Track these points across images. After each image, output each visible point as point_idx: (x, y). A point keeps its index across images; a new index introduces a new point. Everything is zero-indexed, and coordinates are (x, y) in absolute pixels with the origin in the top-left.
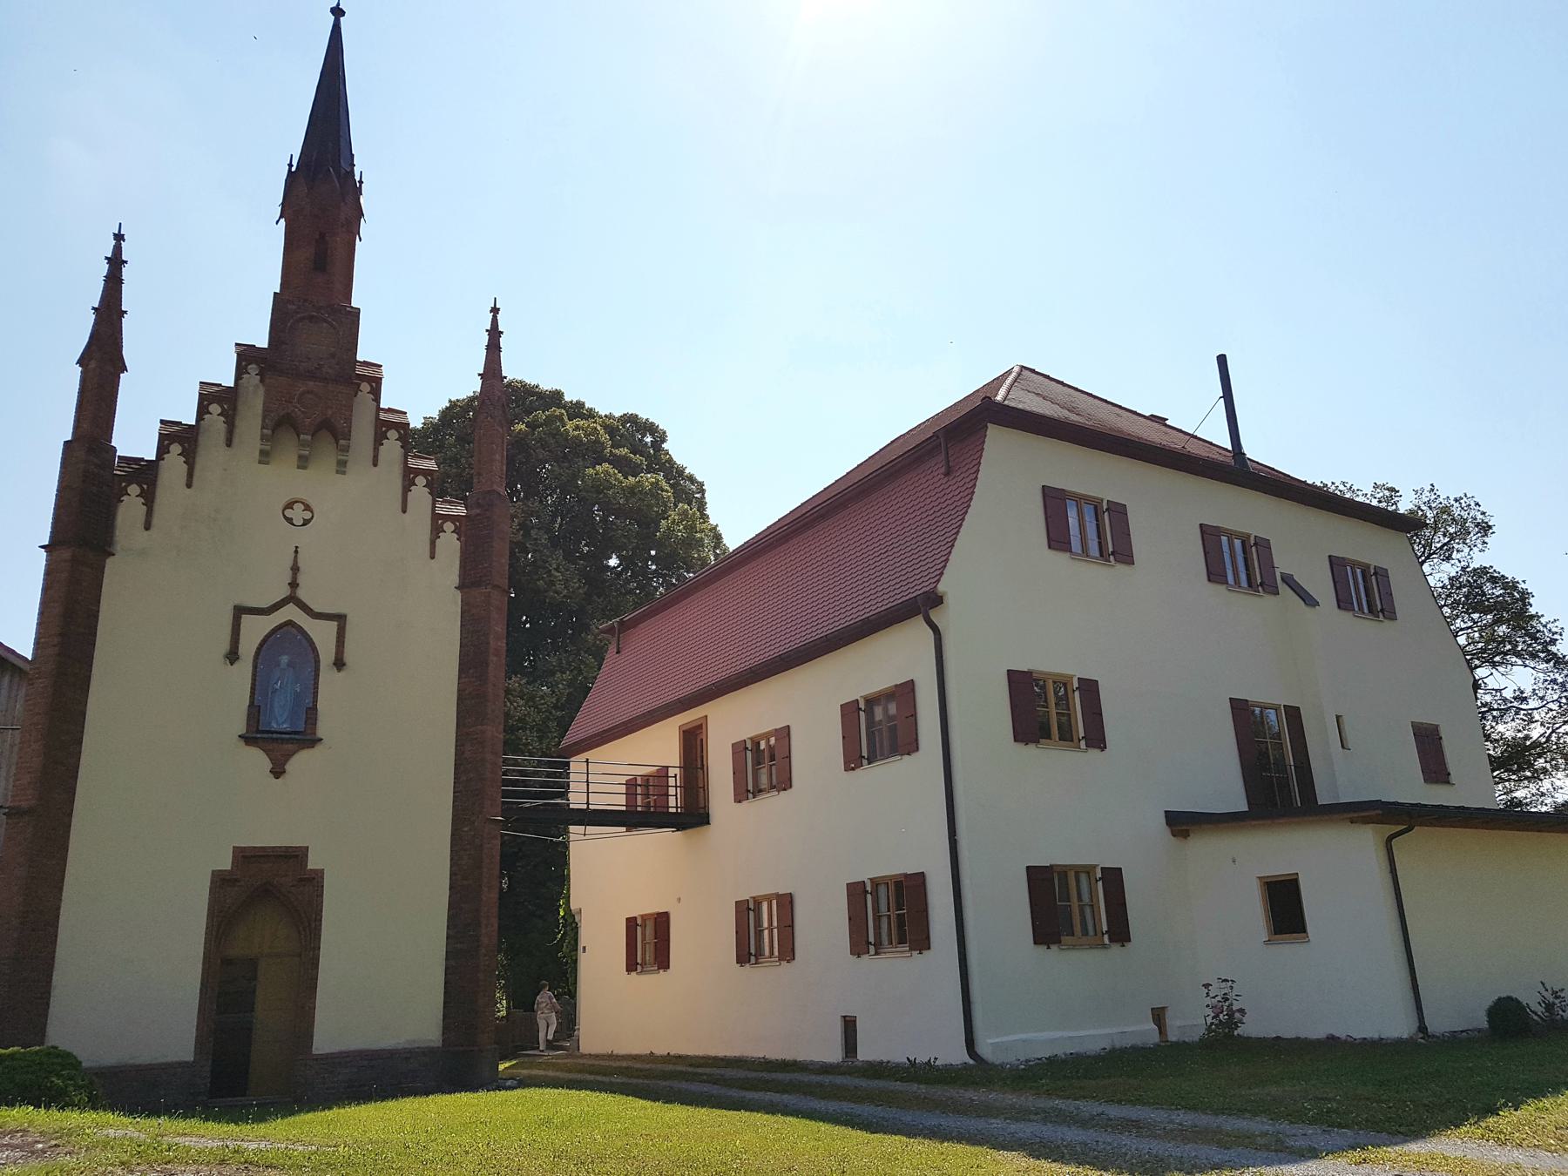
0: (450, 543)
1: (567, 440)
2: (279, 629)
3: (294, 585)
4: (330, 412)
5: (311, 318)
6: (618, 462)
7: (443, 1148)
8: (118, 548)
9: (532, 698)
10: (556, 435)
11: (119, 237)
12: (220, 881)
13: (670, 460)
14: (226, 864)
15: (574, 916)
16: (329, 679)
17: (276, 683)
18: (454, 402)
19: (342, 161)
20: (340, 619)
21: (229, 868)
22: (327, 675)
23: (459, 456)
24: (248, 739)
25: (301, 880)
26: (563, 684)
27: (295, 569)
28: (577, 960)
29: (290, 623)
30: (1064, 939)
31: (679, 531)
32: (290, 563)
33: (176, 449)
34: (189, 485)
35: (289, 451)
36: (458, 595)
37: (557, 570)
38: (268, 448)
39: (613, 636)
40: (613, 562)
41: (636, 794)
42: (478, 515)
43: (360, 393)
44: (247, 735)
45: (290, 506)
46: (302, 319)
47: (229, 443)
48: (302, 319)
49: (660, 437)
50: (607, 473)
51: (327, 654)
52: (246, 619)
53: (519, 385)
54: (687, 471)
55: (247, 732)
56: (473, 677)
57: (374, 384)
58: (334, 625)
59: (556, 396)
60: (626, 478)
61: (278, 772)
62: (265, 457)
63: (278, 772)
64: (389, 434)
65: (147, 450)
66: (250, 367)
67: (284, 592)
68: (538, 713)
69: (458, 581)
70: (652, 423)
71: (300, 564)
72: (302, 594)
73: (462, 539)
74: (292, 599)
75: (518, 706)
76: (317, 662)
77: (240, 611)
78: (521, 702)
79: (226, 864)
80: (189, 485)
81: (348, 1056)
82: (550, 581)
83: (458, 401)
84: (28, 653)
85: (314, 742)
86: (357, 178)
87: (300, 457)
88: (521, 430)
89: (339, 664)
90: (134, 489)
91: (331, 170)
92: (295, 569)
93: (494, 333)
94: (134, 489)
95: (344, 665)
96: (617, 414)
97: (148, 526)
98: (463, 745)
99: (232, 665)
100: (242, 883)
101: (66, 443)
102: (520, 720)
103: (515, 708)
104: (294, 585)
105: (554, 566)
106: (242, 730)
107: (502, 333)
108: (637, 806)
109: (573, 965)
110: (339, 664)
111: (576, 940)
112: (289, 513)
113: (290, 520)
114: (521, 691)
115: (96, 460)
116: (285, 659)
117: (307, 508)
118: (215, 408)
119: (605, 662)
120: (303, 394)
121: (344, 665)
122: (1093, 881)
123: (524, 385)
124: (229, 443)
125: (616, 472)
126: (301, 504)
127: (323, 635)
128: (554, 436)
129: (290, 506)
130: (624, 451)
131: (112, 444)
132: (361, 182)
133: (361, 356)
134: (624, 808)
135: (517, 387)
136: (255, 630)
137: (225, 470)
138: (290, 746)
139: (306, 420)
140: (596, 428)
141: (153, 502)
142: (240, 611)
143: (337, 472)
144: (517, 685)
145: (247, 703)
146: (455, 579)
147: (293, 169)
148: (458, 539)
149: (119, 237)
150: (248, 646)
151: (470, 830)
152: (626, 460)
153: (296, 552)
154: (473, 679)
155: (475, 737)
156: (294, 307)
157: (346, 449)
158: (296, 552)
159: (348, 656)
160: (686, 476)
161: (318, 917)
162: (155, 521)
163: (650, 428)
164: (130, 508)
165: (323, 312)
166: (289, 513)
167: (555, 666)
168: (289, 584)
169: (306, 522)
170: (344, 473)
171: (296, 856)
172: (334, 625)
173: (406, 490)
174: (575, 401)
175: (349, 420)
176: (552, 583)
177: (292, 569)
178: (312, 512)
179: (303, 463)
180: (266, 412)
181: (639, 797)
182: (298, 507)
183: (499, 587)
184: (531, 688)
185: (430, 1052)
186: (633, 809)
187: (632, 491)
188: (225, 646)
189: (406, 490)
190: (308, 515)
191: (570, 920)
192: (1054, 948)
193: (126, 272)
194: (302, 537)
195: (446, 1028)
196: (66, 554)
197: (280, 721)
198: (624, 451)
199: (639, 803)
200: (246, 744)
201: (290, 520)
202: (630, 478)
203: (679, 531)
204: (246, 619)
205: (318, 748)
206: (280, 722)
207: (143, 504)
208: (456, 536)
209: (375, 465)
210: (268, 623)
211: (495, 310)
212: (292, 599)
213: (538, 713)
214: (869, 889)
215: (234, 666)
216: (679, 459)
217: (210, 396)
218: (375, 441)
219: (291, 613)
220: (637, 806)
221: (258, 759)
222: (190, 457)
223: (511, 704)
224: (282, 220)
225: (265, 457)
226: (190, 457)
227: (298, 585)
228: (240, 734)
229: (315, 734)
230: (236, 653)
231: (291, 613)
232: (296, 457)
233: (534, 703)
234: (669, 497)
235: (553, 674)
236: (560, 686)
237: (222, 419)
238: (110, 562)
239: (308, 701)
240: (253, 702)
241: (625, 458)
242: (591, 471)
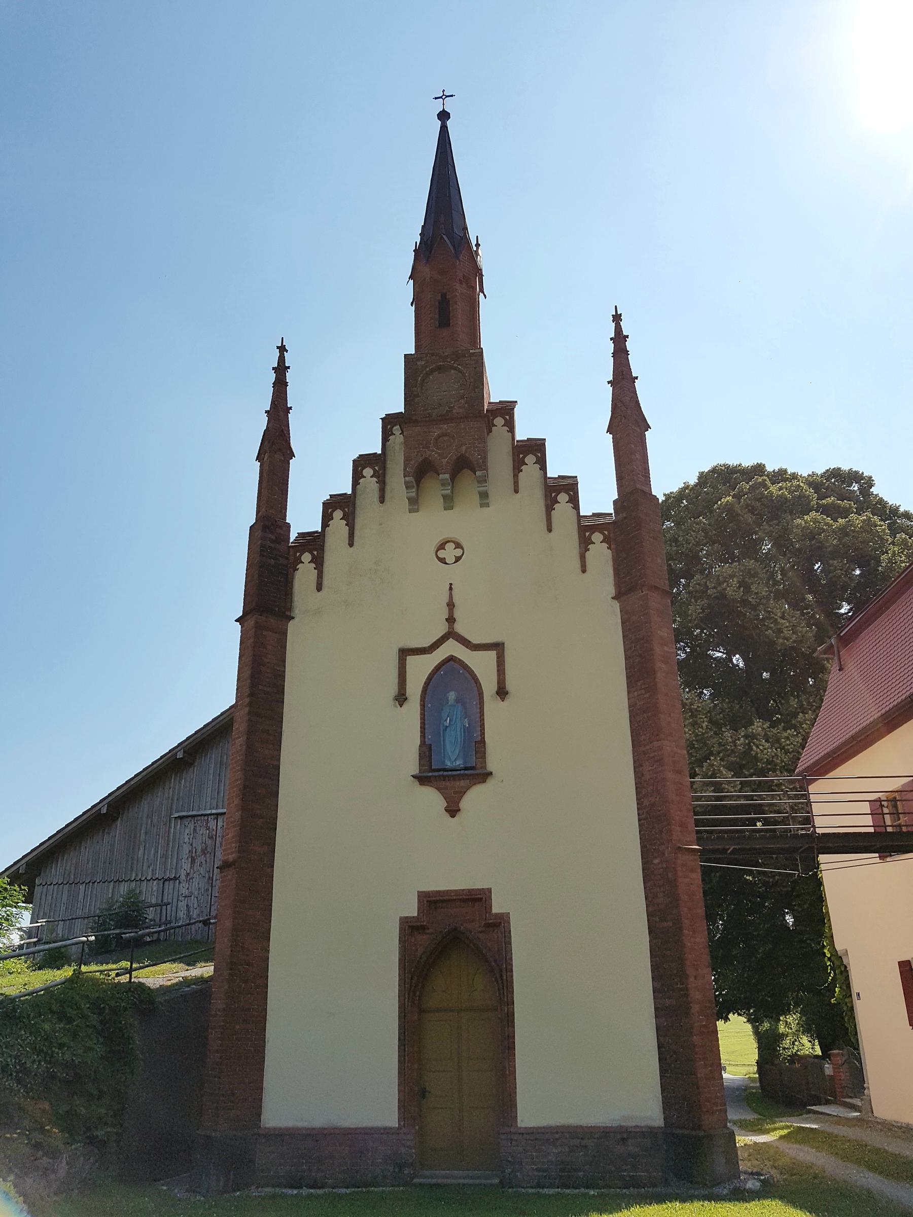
1: (773, 501)
2: (443, 665)
3: (451, 620)
4: (464, 448)
5: (440, 369)
6: (826, 510)
8: (297, 612)
9: (778, 741)
10: (761, 498)
11: (282, 349)
13: (881, 501)
14: (412, 910)
15: (841, 957)
16: (493, 709)
17: (446, 720)
18: (668, 494)
19: (455, 229)
20: (498, 647)
21: (416, 915)
22: (492, 706)
23: (676, 536)
24: (422, 779)
25: (488, 925)
26: (806, 724)
27: (451, 605)
28: (852, 1007)
29: (451, 659)
31: (902, 562)
32: (446, 600)
33: (338, 514)
34: (351, 544)
36: (616, 605)
37: (783, 617)
38: (414, 495)
39: (833, 653)
40: (845, 609)
41: (883, 814)
42: (625, 518)
43: (494, 428)
44: (420, 775)
45: (442, 547)
46: (432, 371)
47: (382, 500)
48: (432, 371)
49: (869, 482)
50: (815, 521)
51: (489, 686)
52: (411, 660)
53: (723, 468)
54: (902, 509)
55: (420, 772)
56: (641, 689)
57: (507, 417)
58: (493, 654)
59: (759, 469)
60: (835, 521)
61: (453, 811)
62: (414, 504)
63: (453, 811)
64: (526, 460)
66: (395, 428)
68: (786, 754)
69: (614, 592)
70: (855, 471)
71: (456, 600)
72: (459, 628)
73: (612, 546)
74: (451, 634)
75: (765, 749)
76: (481, 694)
77: (404, 653)
78: (767, 745)
79: (412, 910)
80: (351, 544)
81: (557, 1133)
82: (777, 628)
83: (671, 493)
85: (484, 776)
86: (474, 243)
87: (445, 497)
88: (728, 501)
89: (502, 692)
90: (306, 557)
91: (446, 239)
92: (451, 605)
93: (620, 339)
95: (507, 693)
96: (820, 471)
97: (319, 588)
98: (641, 765)
99: (401, 707)
100: (431, 931)
102: (769, 762)
103: (762, 751)
104: (451, 620)
105: (779, 614)
106: (416, 771)
107: (627, 337)
108: (886, 826)
109: (849, 1013)
111: (848, 986)
112: (441, 554)
113: (443, 561)
114: (766, 734)
115: (270, 536)
116: (452, 696)
117: (458, 546)
118: (368, 472)
119: (829, 683)
120: (439, 436)
121: (507, 693)
123: (727, 467)
124: (382, 500)
125: (825, 517)
126: (452, 544)
128: (759, 500)
129: (442, 547)
130: (830, 500)
131: (287, 521)
132: (478, 245)
134: (872, 830)
135: (721, 470)
137: (381, 524)
138: (463, 783)
139: (443, 460)
140: (799, 485)
141: (322, 565)
142: (404, 653)
143: (482, 506)
144: (760, 729)
145: (418, 742)
146: (611, 590)
148: (608, 548)
149: (282, 349)
150: (415, 688)
151: (661, 862)
152: (834, 508)
153: (451, 589)
154: (643, 691)
155: (652, 755)
156: (423, 363)
157: (483, 480)
158: (451, 589)
160: (902, 514)
161: (509, 967)
162: (326, 582)
163: (855, 476)
164: (305, 573)
165: (449, 360)
166: (441, 554)
167: (797, 708)
168: (447, 619)
169: (458, 559)
170: (488, 505)
172: (493, 654)
174: (777, 470)
176: (780, 631)
177: (448, 605)
178: (463, 549)
179: (449, 502)
180: (407, 460)
181: (887, 817)
182: (450, 546)
183: (657, 588)
184: (775, 730)
185: (650, 1132)
186: (883, 830)
187: (843, 532)
188: (394, 689)
190: (458, 552)
191: (837, 963)
193: (290, 376)
194: (452, 573)
195: (667, 1104)
196: (251, 622)
197: (453, 758)
198: (830, 500)
199: (888, 822)
200: (420, 784)
201: (443, 561)
202: (840, 520)
203: (902, 562)
204: (411, 660)
205: (490, 784)
206: (453, 760)
207: (315, 569)
208: (606, 545)
209: (516, 491)
210: (430, 662)
211: (617, 318)
212: (451, 634)
213: (786, 754)
215: (404, 706)
216: (891, 499)
217: (361, 463)
218: (514, 468)
219: (451, 648)
220: (886, 826)
222: (350, 519)
223: (758, 747)
224: (411, 282)
225: (414, 504)
226: (350, 519)
227: (455, 620)
228: (412, 774)
229: (485, 767)
230: (404, 695)
231: (451, 648)
232: (442, 499)
233: (780, 744)
234: (884, 530)
235: (795, 715)
236: (804, 726)
237: (375, 479)
238: (291, 625)
239: (477, 735)
240: (425, 742)
241: (833, 504)
242: (799, 521)
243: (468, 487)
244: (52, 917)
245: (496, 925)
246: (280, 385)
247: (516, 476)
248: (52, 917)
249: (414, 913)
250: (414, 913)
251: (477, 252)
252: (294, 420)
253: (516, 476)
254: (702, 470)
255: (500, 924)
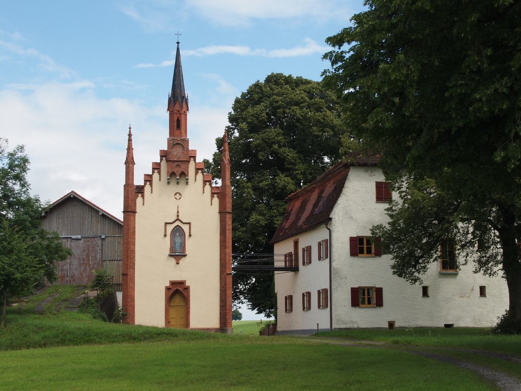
0: (216, 200)
3: (178, 216)
7: (320, 376)
12: (168, 289)
20: (189, 223)
27: (178, 212)
29: (178, 225)
30: (361, 305)
35: (173, 182)
61: (178, 263)
65: (142, 183)
67: (175, 218)
71: (179, 211)
72: (180, 218)
74: (178, 219)
84: (122, 220)
85: (185, 256)
89: (190, 236)
94: (140, 195)
101: (124, 185)
104: (178, 216)
110: (190, 236)
117: (180, 194)
122: (373, 291)
127: (186, 228)
129: (176, 194)
132: (187, 97)
133: (190, 148)
136: (170, 228)
147: (170, 97)
159: (192, 234)
171: (182, 283)
172: (188, 225)
173: (204, 187)
175: (188, 171)
182: (178, 194)
188: (163, 234)
189: (204, 187)
192: (357, 308)
193: (133, 138)
212: (178, 219)
214: (321, 292)
221: (173, 261)
224: (168, 111)
229: (185, 253)
243: (182, 181)
244: (121, 289)
245: (187, 288)
246: (130, 140)
247: (196, 177)
248: (121, 289)
249: (169, 285)
250: (169, 285)
251: (187, 98)
252: (133, 142)
253: (196, 177)
254: (355, 14)
255: (187, 289)
